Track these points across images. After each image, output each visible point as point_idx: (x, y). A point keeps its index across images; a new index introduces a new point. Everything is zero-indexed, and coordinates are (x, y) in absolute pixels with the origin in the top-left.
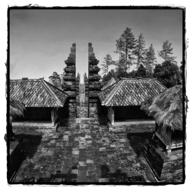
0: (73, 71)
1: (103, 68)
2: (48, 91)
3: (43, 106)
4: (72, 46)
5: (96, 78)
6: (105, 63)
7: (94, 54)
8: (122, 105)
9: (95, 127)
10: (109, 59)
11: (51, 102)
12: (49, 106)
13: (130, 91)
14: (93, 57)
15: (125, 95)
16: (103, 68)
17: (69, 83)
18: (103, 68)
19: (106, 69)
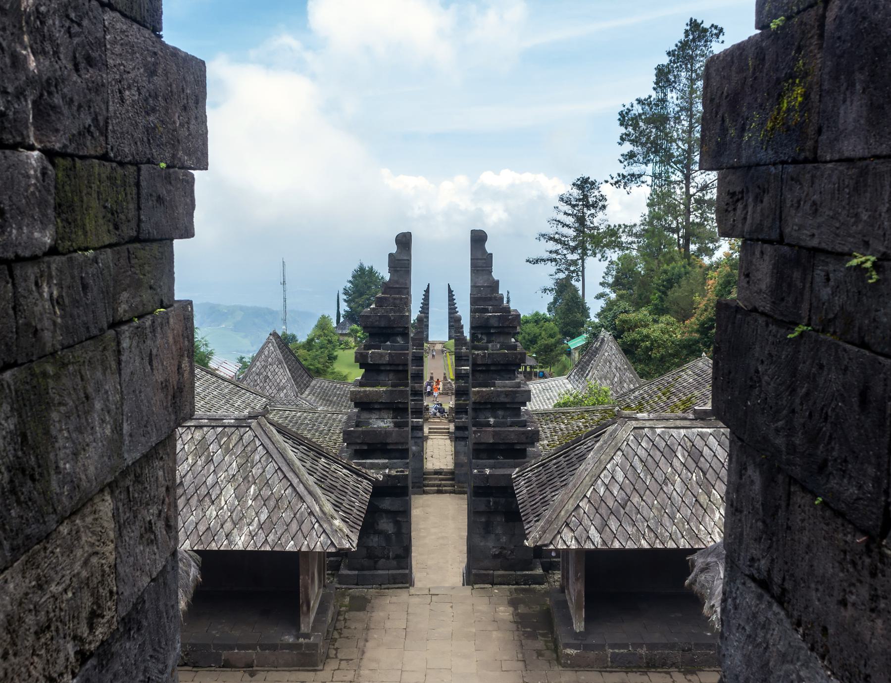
0: (398, 365)
1: (556, 252)
2: (290, 475)
3: (268, 548)
4: (394, 249)
5: (503, 399)
6: (565, 225)
7: (495, 285)
8: (617, 545)
9: (461, 418)
10: (588, 206)
11: (304, 527)
12: (290, 547)
13: (658, 474)
14: (490, 299)
15: (636, 499)
16: (554, 256)
17: (382, 423)
18: (554, 256)
19: (574, 263)
